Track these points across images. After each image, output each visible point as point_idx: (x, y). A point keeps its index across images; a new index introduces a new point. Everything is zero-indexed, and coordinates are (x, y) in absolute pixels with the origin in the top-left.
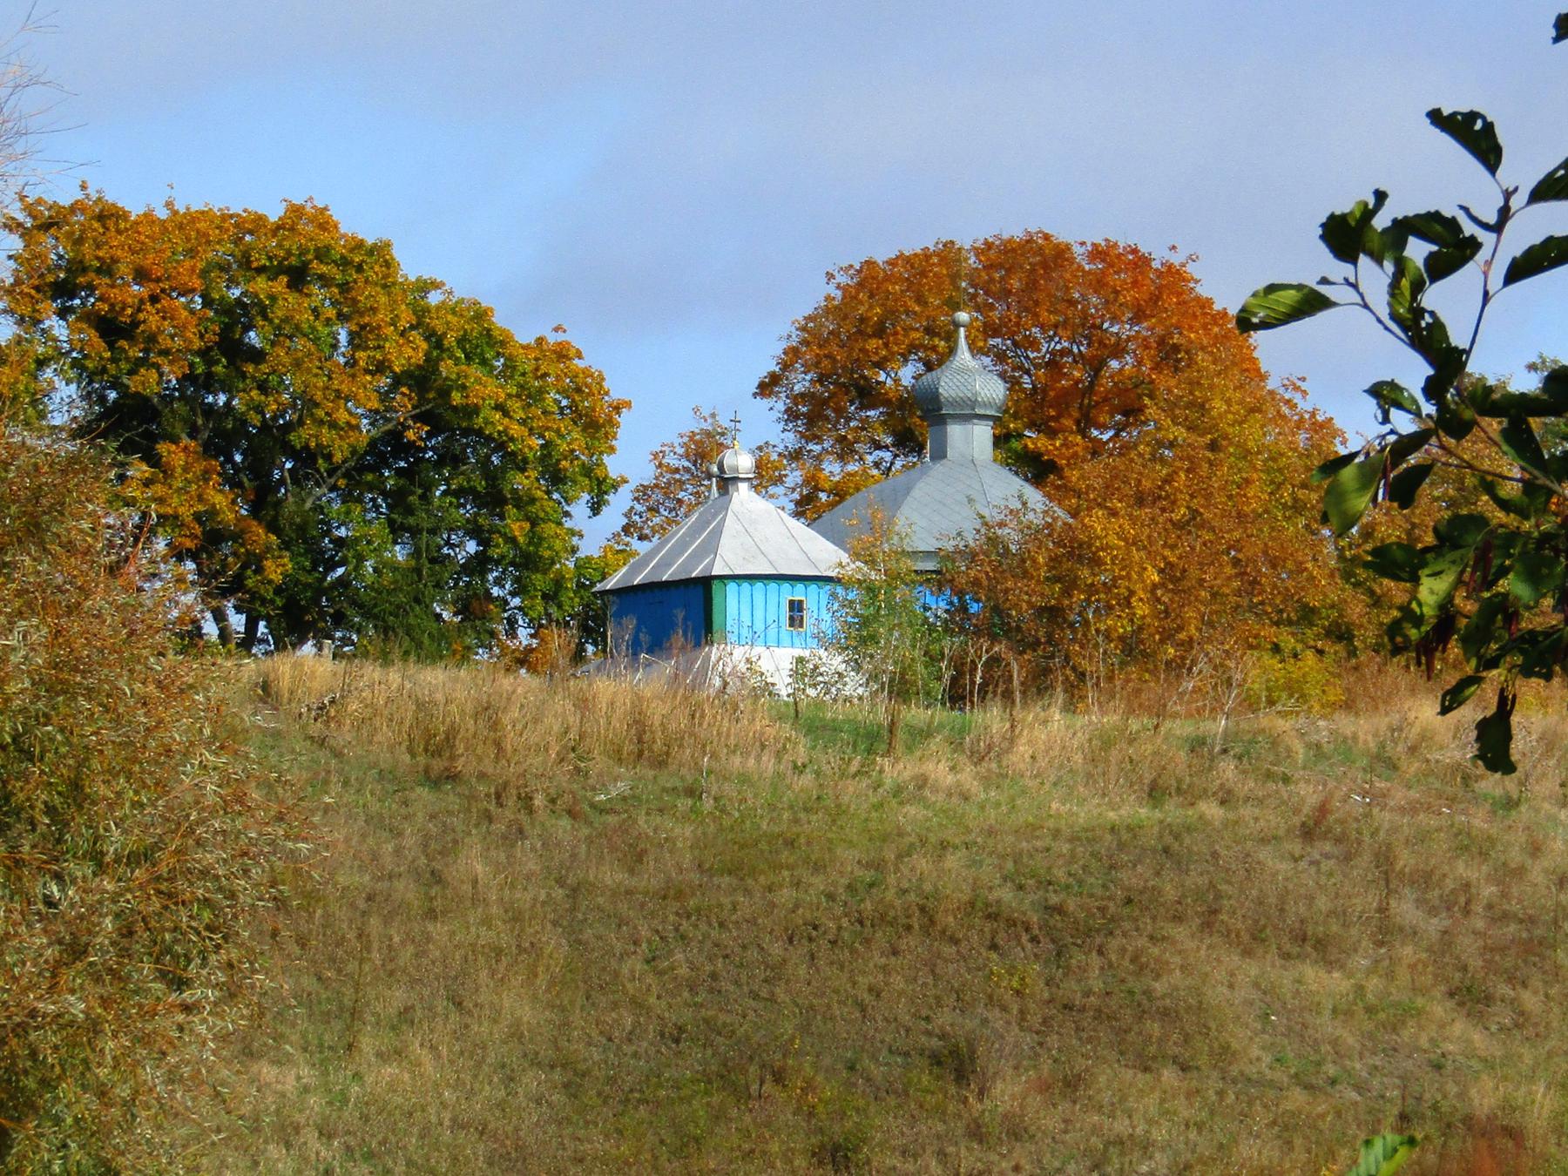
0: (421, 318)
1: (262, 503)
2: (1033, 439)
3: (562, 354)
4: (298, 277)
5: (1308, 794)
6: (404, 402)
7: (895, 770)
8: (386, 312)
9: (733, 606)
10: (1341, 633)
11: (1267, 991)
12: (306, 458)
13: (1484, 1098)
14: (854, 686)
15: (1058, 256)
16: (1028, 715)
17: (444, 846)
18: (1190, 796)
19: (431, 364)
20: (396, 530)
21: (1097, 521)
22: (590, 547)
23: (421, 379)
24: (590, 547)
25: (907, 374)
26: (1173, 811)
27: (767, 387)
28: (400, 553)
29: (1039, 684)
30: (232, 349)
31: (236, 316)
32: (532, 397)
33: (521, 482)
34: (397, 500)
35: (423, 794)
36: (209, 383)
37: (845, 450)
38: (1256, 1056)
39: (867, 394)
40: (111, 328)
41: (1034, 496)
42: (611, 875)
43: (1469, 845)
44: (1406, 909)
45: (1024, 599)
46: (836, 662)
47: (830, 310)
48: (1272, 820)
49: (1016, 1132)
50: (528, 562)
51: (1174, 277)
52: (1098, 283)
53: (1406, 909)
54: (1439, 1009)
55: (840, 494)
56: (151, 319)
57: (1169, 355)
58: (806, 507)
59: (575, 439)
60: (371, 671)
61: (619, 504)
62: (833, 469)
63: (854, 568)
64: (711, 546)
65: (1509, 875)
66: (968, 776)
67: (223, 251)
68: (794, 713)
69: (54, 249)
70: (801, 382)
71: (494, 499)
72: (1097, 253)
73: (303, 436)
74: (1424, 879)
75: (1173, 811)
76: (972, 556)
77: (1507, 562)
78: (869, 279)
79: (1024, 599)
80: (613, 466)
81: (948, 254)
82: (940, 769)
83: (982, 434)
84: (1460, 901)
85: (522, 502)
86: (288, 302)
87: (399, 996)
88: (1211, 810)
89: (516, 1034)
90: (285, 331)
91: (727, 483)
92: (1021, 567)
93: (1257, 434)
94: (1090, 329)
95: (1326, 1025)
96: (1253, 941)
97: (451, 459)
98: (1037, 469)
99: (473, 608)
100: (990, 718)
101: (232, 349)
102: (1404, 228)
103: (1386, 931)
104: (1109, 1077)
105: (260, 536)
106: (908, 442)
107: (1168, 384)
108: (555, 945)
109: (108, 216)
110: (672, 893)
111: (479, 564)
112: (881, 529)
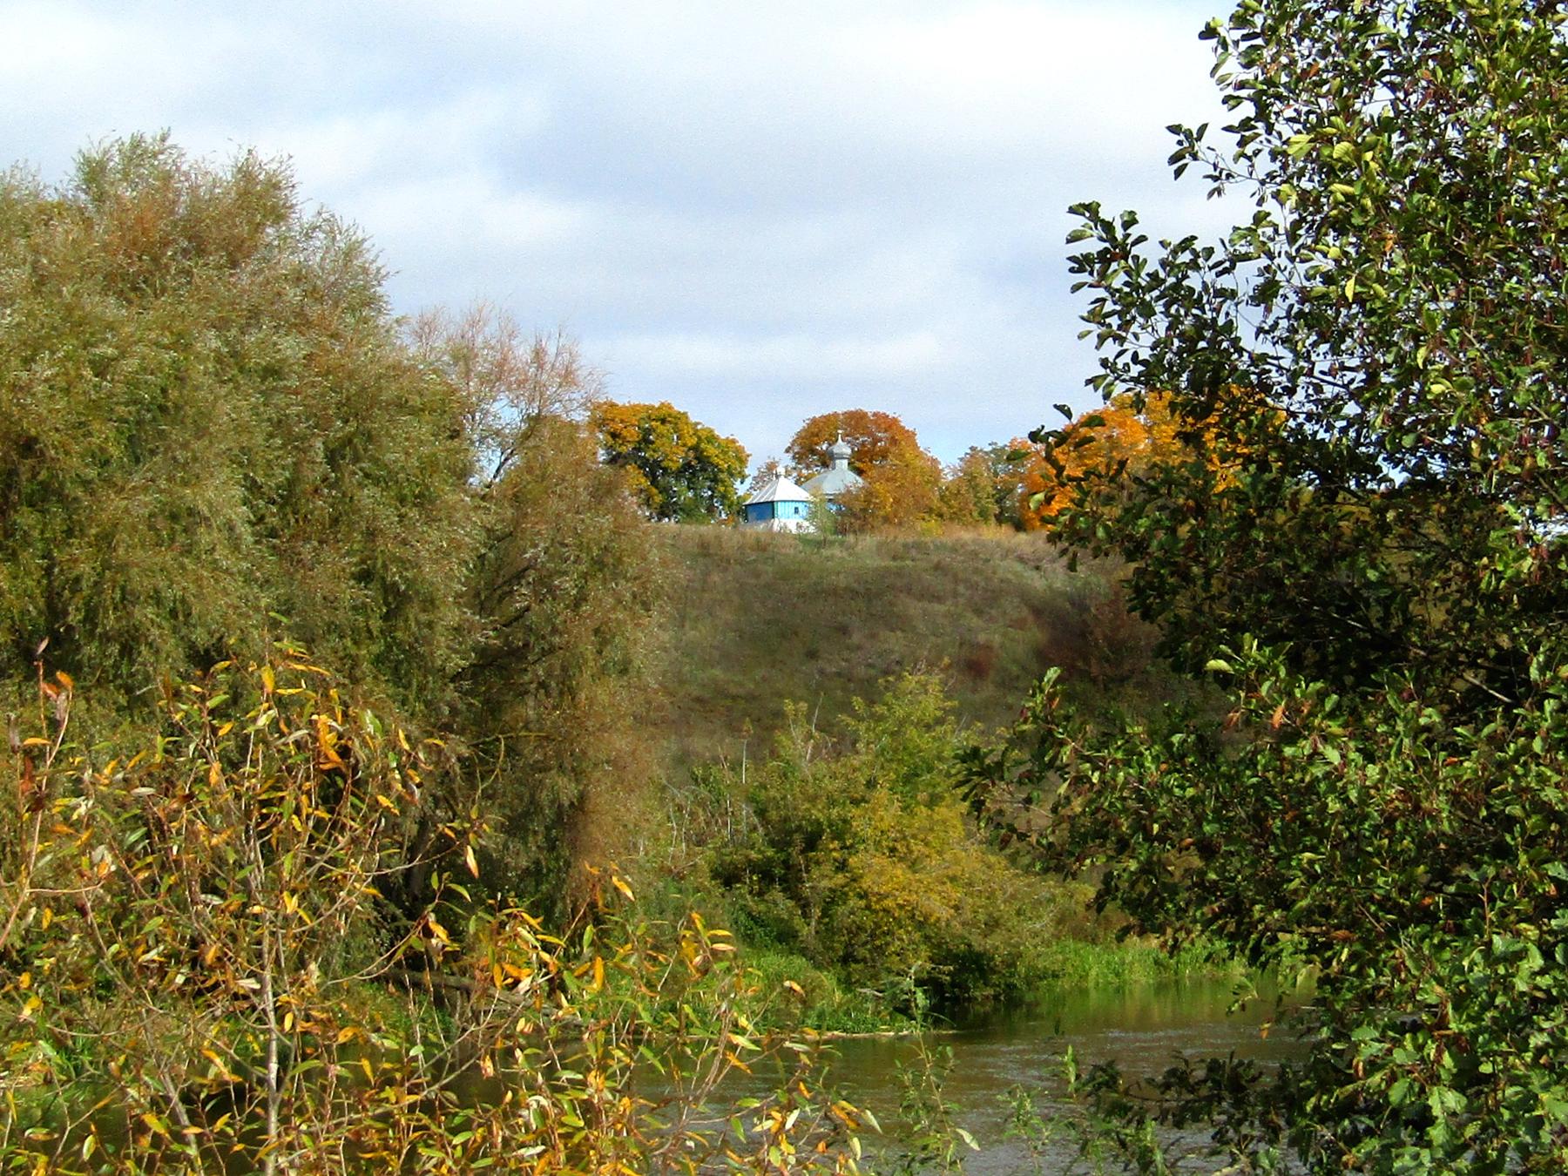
0: (696, 432)
1: (654, 482)
2: (858, 464)
3: (734, 441)
4: (663, 421)
5: (935, 559)
6: (691, 454)
7: (825, 552)
8: (686, 430)
9: (780, 508)
10: (941, 515)
11: (925, 612)
12: (665, 469)
13: (982, 638)
14: (812, 529)
15: (865, 414)
16: (861, 537)
17: (706, 574)
18: (902, 559)
19: (698, 443)
20: (689, 488)
21: (877, 485)
22: (741, 493)
23: (695, 448)
24: (741, 493)
25: (824, 447)
26: (898, 563)
27: (787, 451)
28: (690, 494)
29: (862, 530)
30: (646, 441)
31: (648, 431)
32: (725, 453)
33: (722, 476)
34: (689, 481)
35: (700, 559)
36: (639, 450)
37: (808, 467)
38: (922, 628)
39: (813, 452)
40: (614, 435)
41: (860, 480)
42: (753, 581)
43: (976, 571)
44: (961, 589)
45: (857, 507)
46: (806, 524)
47: (804, 430)
48: (924, 565)
49: (859, 648)
50: (724, 497)
51: (895, 421)
52: (875, 422)
53: (961, 589)
54: (969, 615)
55: (807, 478)
56: (624, 433)
57: (894, 441)
58: (797, 482)
59: (737, 465)
60: (687, 527)
61: (748, 481)
62: (804, 472)
63: (811, 498)
64: (774, 493)
65: (988, 579)
66: (845, 554)
67: (644, 415)
68: (796, 537)
69: (598, 414)
70: (796, 449)
71: (715, 480)
72: (875, 414)
73: (664, 464)
74: (966, 581)
75: (898, 563)
76: (843, 495)
77: (1353, 665)
78: (814, 421)
79: (857, 507)
80: (747, 471)
81: (835, 415)
82: (837, 551)
83: (845, 462)
84: (973, 587)
85: (723, 481)
86: (662, 429)
87: (695, 613)
88: (908, 562)
89: (726, 623)
90: (662, 436)
91: (777, 476)
92: (857, 498)
93: (918, 463)
94: (871, 434)
95: (940, 620)
96: (921, 597)
97: (703, 470)
98: (860, 472)
99: (711, 510)
100: (851, 538)
101: (646, 441)
102: (1049, 434)
103: (955, 595)
104: (884, 634)
105: (655, 491)
106: (825, 465)
107: (893, 449)
108: (736, 599)
109: (613, 405)
110: (767, 586)
111: (711, 497)
112: (818, 488)
